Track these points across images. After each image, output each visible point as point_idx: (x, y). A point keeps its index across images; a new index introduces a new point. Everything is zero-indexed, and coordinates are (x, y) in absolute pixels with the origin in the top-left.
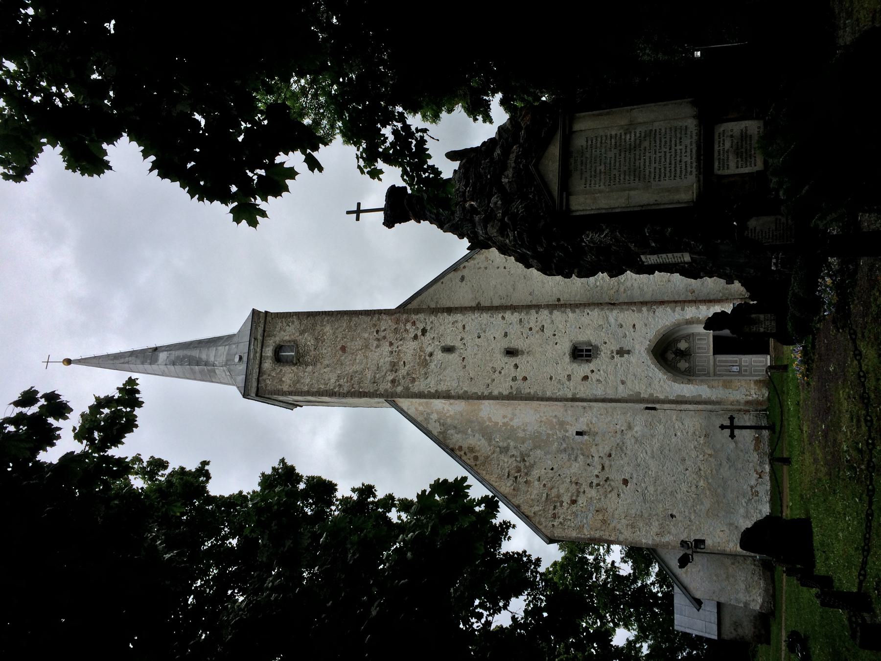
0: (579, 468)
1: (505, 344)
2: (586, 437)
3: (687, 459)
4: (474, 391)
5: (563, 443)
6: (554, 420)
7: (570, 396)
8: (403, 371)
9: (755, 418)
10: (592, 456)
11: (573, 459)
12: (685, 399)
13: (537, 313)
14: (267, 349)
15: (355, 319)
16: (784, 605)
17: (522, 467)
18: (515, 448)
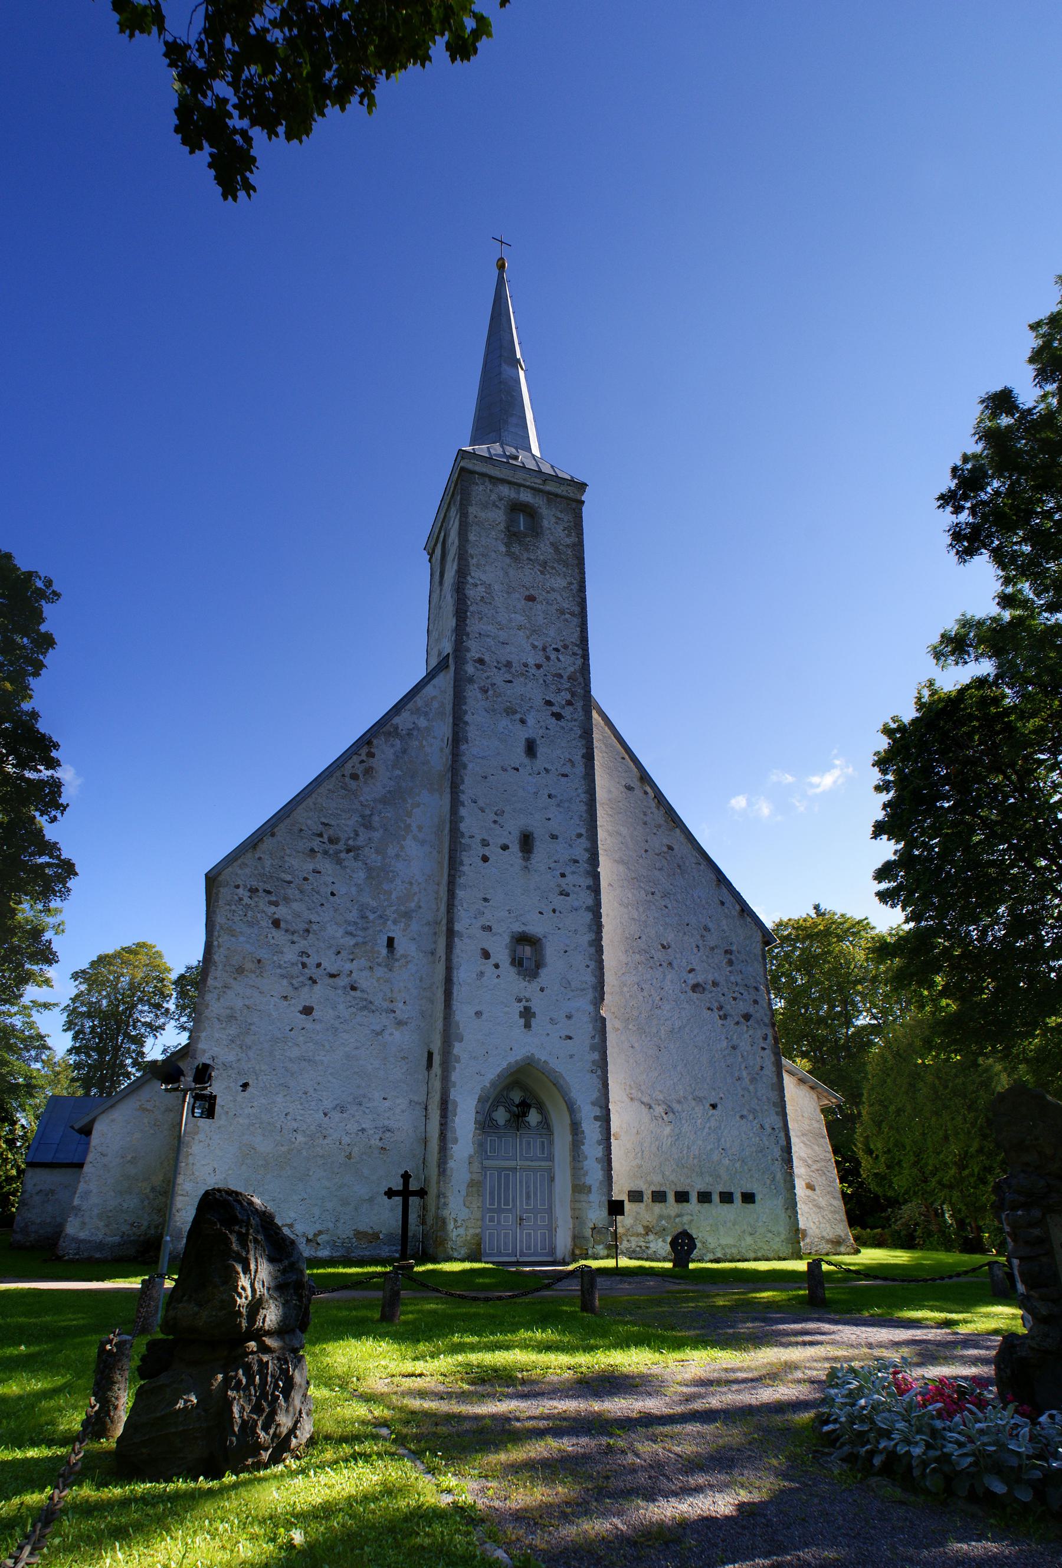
1: (540, 833)
2: (384, 951)
3: (345, 1115)
4: (466, 779)
5: (376, 915)
6: (413, 905)
7: (457, 927)
8: (499, 678)
10: (352, 960)
12: (449, 1114)
13: (588, 887)
14: (529, 495)
15: (576, 621)
16: (32, 1453)
17: (337, 847)
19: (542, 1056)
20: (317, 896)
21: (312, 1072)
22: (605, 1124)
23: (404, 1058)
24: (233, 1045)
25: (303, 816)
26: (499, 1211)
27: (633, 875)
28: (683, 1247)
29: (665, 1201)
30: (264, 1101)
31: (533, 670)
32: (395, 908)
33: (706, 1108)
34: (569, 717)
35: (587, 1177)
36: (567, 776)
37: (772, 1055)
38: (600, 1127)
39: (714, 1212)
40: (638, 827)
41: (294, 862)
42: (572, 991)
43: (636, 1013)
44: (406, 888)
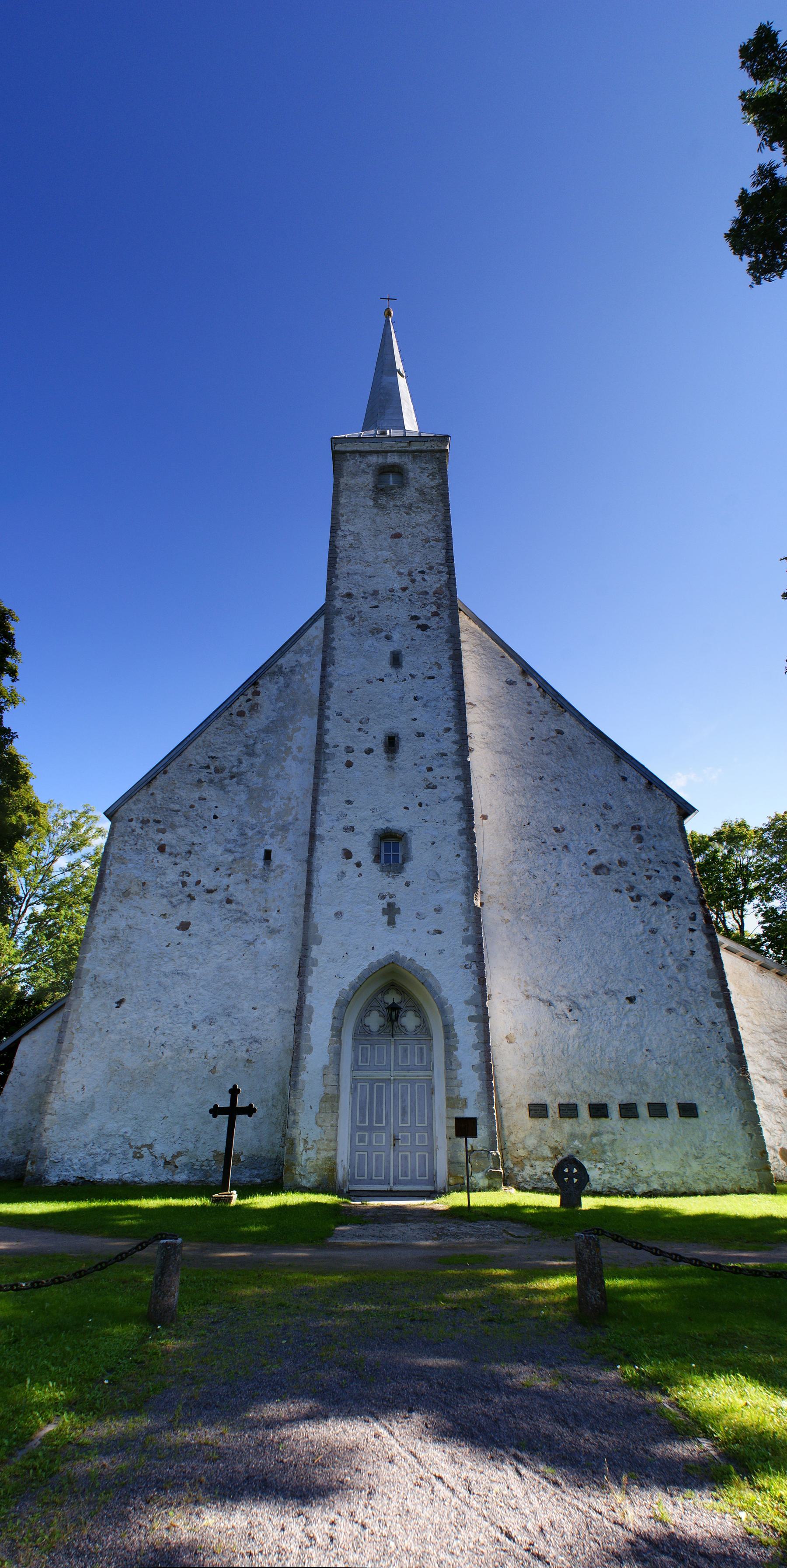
0: (214, 856)
2: (261, 864)
3: (213, 1027)
4: (332, 696)
6: (290, 818)
7: (319, 831)
8: (365, 606)
9: (274, 1156)
10: (230, 875)
11: (229, 846)
12: (304, 1021)
13: (457, 778)
14: (396, 457)
17: (222, 775)
18: (252, 765)
19: (407, 953)
20: (200, 820)
21: (184, 985)
22: (482, 1025)
23: (274, 966)
24: (114, 964)
25: (194, 755)
26: (371, 1129)
27: (518, 763)
28: (571, 1180)
29: (576, 1116)
30: (135, 1016)
31: (399, 593)
32: (273, 823)
33: (622, 1002)
34: (435, 627)
35: (462, 1089)
36: (433, 678)
37: (704, 937)
38: (476, 1029)
39: (643, 1129)
40: (522, 717)
41: (183, 793)
42: (441, 883)
43: (528, 903)
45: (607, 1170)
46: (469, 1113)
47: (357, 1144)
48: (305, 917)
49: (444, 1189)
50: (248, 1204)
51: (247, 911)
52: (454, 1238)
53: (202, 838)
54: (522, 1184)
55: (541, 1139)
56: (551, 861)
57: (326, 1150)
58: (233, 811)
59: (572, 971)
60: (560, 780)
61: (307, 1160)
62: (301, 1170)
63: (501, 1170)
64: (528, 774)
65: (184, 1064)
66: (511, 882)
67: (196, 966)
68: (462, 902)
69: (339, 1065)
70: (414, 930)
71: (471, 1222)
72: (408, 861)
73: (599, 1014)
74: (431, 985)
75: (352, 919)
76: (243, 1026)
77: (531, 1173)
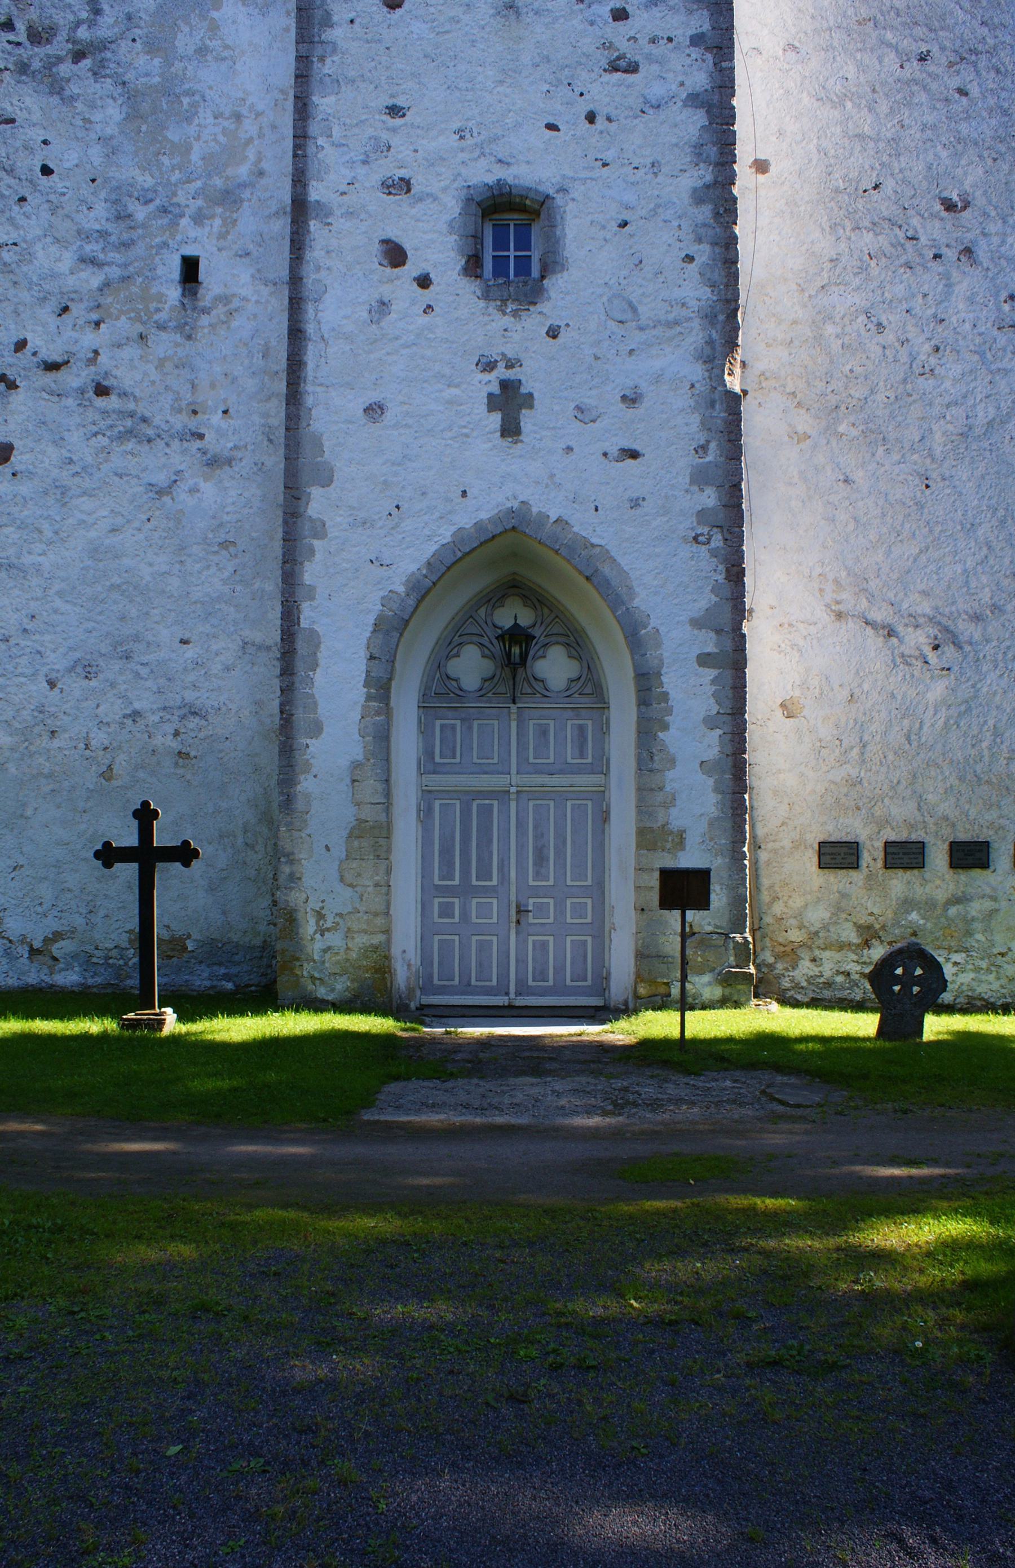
0: (54, 276)
2: (174, 293)
3: (93, 683)
5: (151, 207)
6: (243, 171)
7: (316, 192)
9: (258, 942)
10: (97, 324)
12: (300, 666)
13: (696, 40)
17: (49, 49)
18: (129, 17)
20: (9, 180)
21: (17, 592)
22: (729, 673)
26: (466, 890)
28: (906, 988)
32: (199, 184)
35: (674, 812)
38: (713, 682)
42: (641, 329)
43: (858, 392)
44: (225, 132)
45: (970, 967)
46: (689, 859)
47: (436, 920)
48: (289, 417)
49: (626, 1003)
50: (195, 1034)
51: (148, 414)
52: (653, 1111)
53: (17, 227)
54: (789, 994)
55: (839, 909)
56: (925, 288)
57: (365, 932)
58: (90, 152)
59: (948, 559)
60: (975, 64)
61: (325, 951)
62: (314, 968)
63: (752, 970)
64: (889, 45)
65: (41, 760)
66: (819, 339)
67: (39, 547)
68: (695, 379)
69: (388, 760)
70: (569, 449)
71: (688, 1073)
72: (554, 272)
73: (1000, 657)
74: (608, 582)
75: (410, 421)
76: (162, 681)
77: (811, 973)
